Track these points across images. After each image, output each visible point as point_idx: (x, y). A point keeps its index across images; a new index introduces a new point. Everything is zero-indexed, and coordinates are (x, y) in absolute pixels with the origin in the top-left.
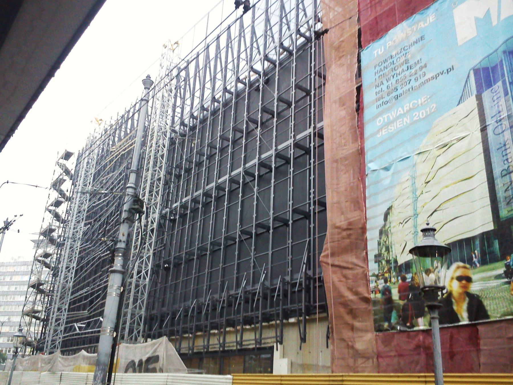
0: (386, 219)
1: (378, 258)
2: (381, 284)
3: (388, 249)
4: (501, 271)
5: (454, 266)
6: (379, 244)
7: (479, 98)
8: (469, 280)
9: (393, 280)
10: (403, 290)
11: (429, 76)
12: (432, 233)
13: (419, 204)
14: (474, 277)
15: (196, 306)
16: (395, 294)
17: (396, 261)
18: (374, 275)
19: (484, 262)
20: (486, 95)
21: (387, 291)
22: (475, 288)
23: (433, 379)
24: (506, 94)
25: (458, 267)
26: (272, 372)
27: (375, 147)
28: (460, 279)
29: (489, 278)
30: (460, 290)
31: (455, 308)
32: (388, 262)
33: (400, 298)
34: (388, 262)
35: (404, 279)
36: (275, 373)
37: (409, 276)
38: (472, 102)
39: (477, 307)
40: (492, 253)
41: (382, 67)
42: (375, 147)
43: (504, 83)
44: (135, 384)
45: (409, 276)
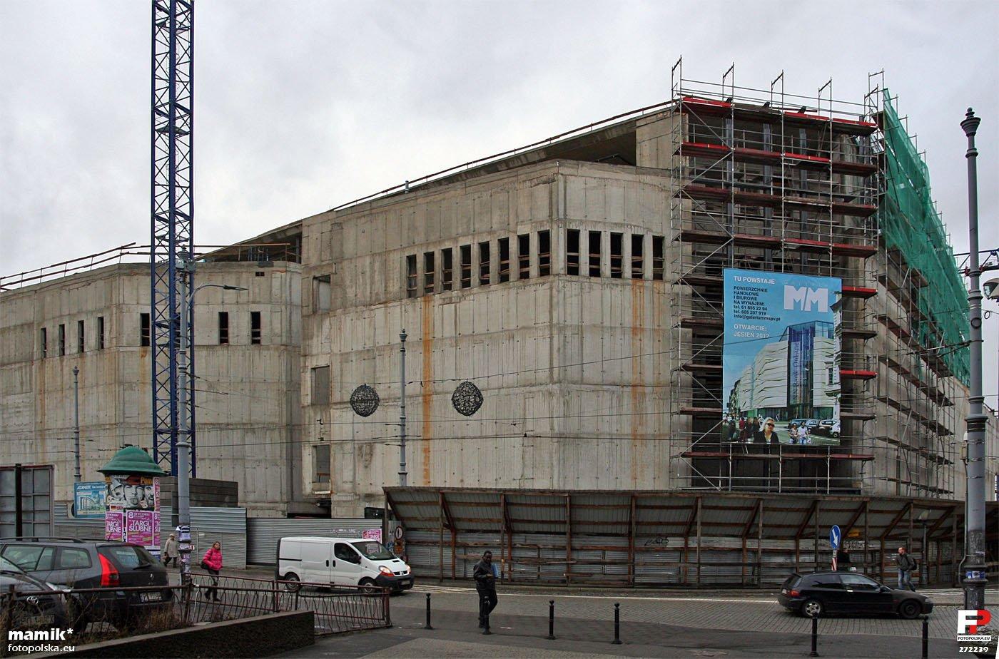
0: (736, 386)
1: (729, 405)
2: (730, 419)
7: (789, 343)
8: (773, 426)
11: (766, 316)
12: (298, 509)
16: (737, 426)
17: (739, 410)
19: (781, 420)
21: (732, 423)
22: (775, 430)
26: (963, 503)
27: (419, 510)
28: (769, 424)
34: (735, 409)
35: (743, 419)
36: (964, 500)
37: (746, 418)
42: (419, 510)
45: (746, 418)
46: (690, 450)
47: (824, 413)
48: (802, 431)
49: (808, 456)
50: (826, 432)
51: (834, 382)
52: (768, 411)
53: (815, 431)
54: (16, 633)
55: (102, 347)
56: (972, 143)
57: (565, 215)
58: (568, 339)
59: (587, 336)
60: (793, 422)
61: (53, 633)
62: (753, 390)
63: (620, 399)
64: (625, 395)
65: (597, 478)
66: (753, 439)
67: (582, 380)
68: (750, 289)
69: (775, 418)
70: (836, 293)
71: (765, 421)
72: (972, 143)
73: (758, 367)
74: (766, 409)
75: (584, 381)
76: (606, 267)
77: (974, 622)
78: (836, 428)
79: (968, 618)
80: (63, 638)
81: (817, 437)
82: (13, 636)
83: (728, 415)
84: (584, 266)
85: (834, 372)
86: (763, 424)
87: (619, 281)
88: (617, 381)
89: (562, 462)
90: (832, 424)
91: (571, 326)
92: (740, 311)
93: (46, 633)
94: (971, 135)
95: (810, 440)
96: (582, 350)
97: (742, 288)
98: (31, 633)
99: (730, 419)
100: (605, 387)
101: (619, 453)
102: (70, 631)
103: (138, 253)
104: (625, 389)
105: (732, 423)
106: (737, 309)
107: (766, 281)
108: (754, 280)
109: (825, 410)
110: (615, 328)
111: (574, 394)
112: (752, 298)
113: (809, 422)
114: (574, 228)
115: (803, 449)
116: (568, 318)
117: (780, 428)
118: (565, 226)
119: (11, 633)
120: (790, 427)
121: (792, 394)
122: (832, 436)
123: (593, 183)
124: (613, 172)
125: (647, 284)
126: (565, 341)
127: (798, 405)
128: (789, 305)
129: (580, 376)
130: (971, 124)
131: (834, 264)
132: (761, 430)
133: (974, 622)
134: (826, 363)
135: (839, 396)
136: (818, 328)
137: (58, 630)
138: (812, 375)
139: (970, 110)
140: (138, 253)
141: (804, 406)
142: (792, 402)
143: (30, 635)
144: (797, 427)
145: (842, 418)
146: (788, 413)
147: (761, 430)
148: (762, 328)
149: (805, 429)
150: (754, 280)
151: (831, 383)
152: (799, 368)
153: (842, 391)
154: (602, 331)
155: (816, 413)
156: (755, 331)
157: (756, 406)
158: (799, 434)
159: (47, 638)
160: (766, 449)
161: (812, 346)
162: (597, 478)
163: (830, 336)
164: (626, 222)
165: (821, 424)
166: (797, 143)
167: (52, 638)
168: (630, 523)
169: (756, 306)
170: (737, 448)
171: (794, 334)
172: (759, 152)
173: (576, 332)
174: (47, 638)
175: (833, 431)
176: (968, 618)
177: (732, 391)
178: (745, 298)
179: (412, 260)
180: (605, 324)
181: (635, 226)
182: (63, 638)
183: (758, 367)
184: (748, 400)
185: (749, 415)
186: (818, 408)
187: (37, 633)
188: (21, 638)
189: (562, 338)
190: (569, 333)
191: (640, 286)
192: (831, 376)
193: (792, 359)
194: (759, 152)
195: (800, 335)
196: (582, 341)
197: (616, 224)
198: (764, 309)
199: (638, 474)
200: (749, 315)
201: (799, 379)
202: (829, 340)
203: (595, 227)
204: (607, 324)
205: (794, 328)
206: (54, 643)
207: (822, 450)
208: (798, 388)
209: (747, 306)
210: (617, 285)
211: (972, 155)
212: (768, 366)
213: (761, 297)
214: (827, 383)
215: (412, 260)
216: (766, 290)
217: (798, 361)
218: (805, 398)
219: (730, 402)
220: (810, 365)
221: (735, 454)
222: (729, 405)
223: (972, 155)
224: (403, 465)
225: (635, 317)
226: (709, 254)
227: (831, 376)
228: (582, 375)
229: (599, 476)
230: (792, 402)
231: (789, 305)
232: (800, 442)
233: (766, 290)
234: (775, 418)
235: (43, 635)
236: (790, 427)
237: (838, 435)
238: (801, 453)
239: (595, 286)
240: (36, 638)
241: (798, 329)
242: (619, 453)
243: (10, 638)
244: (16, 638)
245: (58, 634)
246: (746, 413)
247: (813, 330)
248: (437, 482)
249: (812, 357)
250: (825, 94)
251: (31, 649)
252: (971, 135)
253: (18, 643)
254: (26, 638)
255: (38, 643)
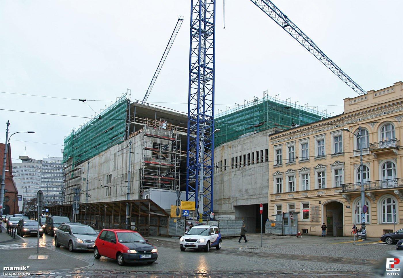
54: (6, 268)
56: (8, 127)
61: (21, 268)
72: (8, 127)
79: (391, 261)
80: (25, 270)
82: (5, 269)
93: (19, 268)
94: (8, 126)
98: (12, 268)
119: (4, 268)
130: (8, 124)
133: (393, 263)
137: (23, 266)
139: (8, 121)
143: (12, 268)
159: (19, 270)
167: (21, 270)
168: (159, 226)
174: (19, 270)
176: (391, 261)
179: (233, 158)
182: (25, 270)
187: (15, 268)
188: (8, 270)
206: (22, 271)
211: (8, 130)
215: (233, 158)
223: (8, 130)
226: (166, 147)
235: (17, 268)
240: (15, 270)
243: (4, 270)
244: (6, 270)
245: (23, 268)
250: (277, 97)
251: (13, 274)
252: (8, 126)
253: (7, 271)
254: (10, 269)
255: (14, 271)
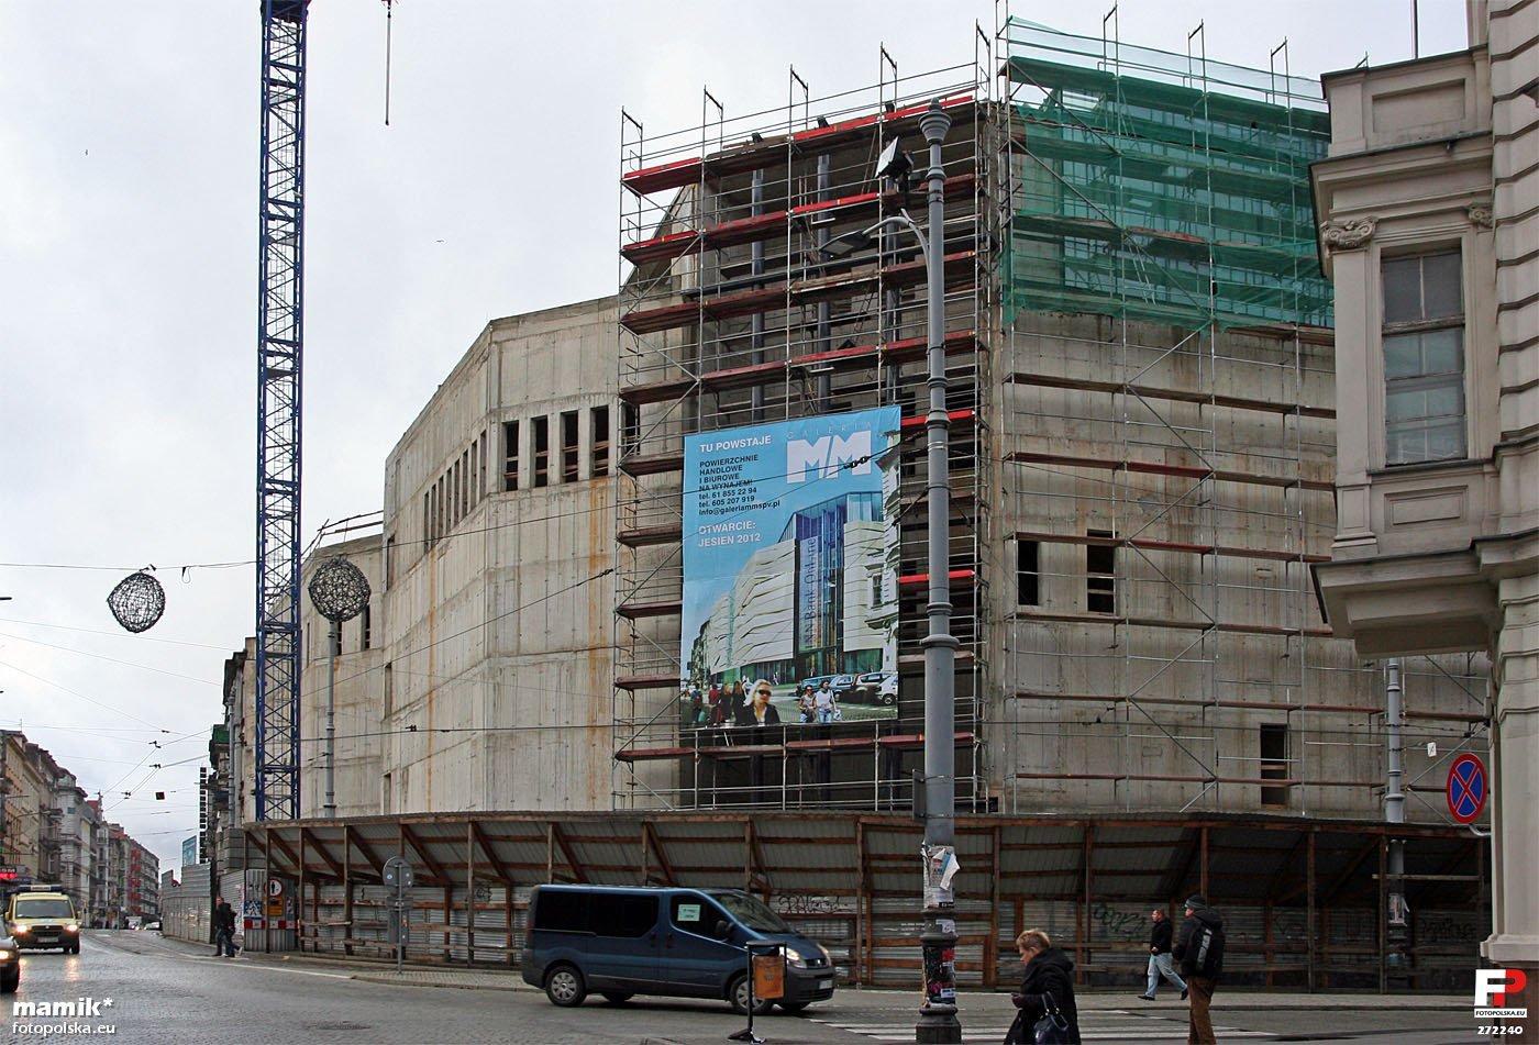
0: (702, 631)
1: (691, 666)
2: (692, 689)
3: (701, 659)
4: (794, 691)
5: (758, 682)
6: (693, 653)
7: (797, 543)
8: (769, 694)
9: (705, 687)
10: (712, 698)
11: (757, 502)
13: (735, 625)
14: (772, 693)
15: (710, 891)
16: (706, 699)
17: (709, 671)
18: (685, 680)
19: (782, 682)
20: (804, 544)
21: (697, 697)
22: (772, 700)
23: (874, 864)
24: (820, 551)
25: (761, 683)
28: (761, 692)
29: (784, 695)
30: (761, 701)
31: (756, 714)
32: (701, 670)
33: (710, 703)
34: (701, 670)
35: (715, 687)
38: (790, 544)
39: (772, 713)
40: (789, 676)
41: (709, 468)
43: (820, 539)
44: (693, 1041)
45: (720, 685)
46: (677, 745)
47: (866, 660)
48: (822, 698)
49: (837, 743)
50: (871, 697)
51: (883, 601)
52: (758, 669)
53: (848, 696)
55: (367, 645)
57: (500, 402)
58: (501, 590)
59: (525, 579)
60: (806, 683)
61: (81, 1005)
62: (732, 634)
63: (571, 671)
64: (580, 664)
65: (539, 800)
66: (734, 719)
67: (518, 650)
68: (727, 461)
69: (771, 680)
70: (888, 434)
71: (754, 687)
73: (740, 594)
74: (757, 666)
75: (521, 651)
76: (554, 471)
77: (1500, 989)
78: (889, 687)
79: (1491, 981)
81: (852, 707)
83: (689, 683)
84: (524, 476)
85: (883, 582)
86: (751, 693)
87: (572, 486)
88: (567, 645)
89: (491, 777)
90: (881, 680)
91: (505, 568)
92: (710, 503)
95: (839, 714)
96: (519, 600)
97: (713, 463)
99: (692, 689)
100: (551, 656)
101: (569, 759)
102: (108, 1002)
103: (337, 532)
104: (579, 655)
105: (697, 697)
106: (703, 501)
107: (756, 442)
108: (734, 444)
109: (868, 655)
110: (565, 561)
111: (508, 673)
112: (731, 477)
113: (837, 681)
114: (512, 419)
115: (826, 731)
116: (501, 560)
117: (781, 696)
118: (499, 420)
120: (800, 692)
121: (802, 632)
122: (881, 703)
123: (537, 343)
124: (567, 317)
125: (612, 482)
126: (496, 593)
127: (814, 652)
128: (796, 477)
129: (516, 644)
131: (791, 399)
132: (747, 702)
133: (1500, 989)
134: (869, 568)
135: (895, 625)
136: (852, 506)
138: (841, 593)
140: (337, 532)
141: (827, 651)
142: (802, 648)
144: (813, 691)
145: (901, 666)
146: (797, 669)
147: (747, 702)
148: (747, 525)
149: (829, 694)
150: (734, 444)
151: (877, 602)
152: (815, 584)
153: (902, 616)
154: (547, 569)
155: (849, 663)
156: (735, 533)
157: (737, 664)
158: (818, 704)
159: (72, 1013)
160: (760, 737)
161: (841, 539)
162: (539, 800)
163: (877, 517)
164: (582, 392)
165: (859, 682)
166: (812, 184)
167: (81, 1013)
169: (736, 489)
170: (706, 738)
171: (805, 525)
172: (746, 221)
173: (511, 577)
175: (883, 693)
176: (1491, 981)
177: (696, 642)
178: (719, 478)
180: (550, 559)
181: (594, 394)
183: (740, 594)
184: (724, 653)
185: (726, 678)
186: (854, 654)
187: (56, 1005)
189: (493, 590)
190: (501, 581)
191: (602, 488)
192: (877, 591)
193: (803, 571)
194: (746, 221)
195: (820, 526)
196: (519, 589)
197: (568, 398)
198: (751, 491)
199: (598, 791)
200: (726, 506)
201: (816, 603)
202: (872, 525)
203: (539, 411)
204: (553, 557)
205: (807, 514)
207: (865, 730)
208: (815, 621)
209: (721, 491)
210: (569, 493)
212: (758, 589)
213: (748, 471)
214: (870, 604)
216: (755, 458)
217: (815, 573)
218: (828, 637)
219: (693, 659)
220: (837, 576)
221: (705, 749)
222: (691, 666)
224: (331, 794)
225: (593, 540)
227: (877, 591)
228: (519, 642)
229: (541, 797)
230: (802, 648)
231: (796, 477)
232: (819, 720)
233: (755, 458)
234: (771, 680)
236: (800, 692)
237: (893, 700)
238: (822, 738)
239: (537, 502)
240: (56, 1013)
241: (812, 515)
242: (569, 759)
243: (16, 1013)
246: (720, 675)
247: (843, 510)
248: (433, 811)
249: (841, 561)
254: (40, 1012)
